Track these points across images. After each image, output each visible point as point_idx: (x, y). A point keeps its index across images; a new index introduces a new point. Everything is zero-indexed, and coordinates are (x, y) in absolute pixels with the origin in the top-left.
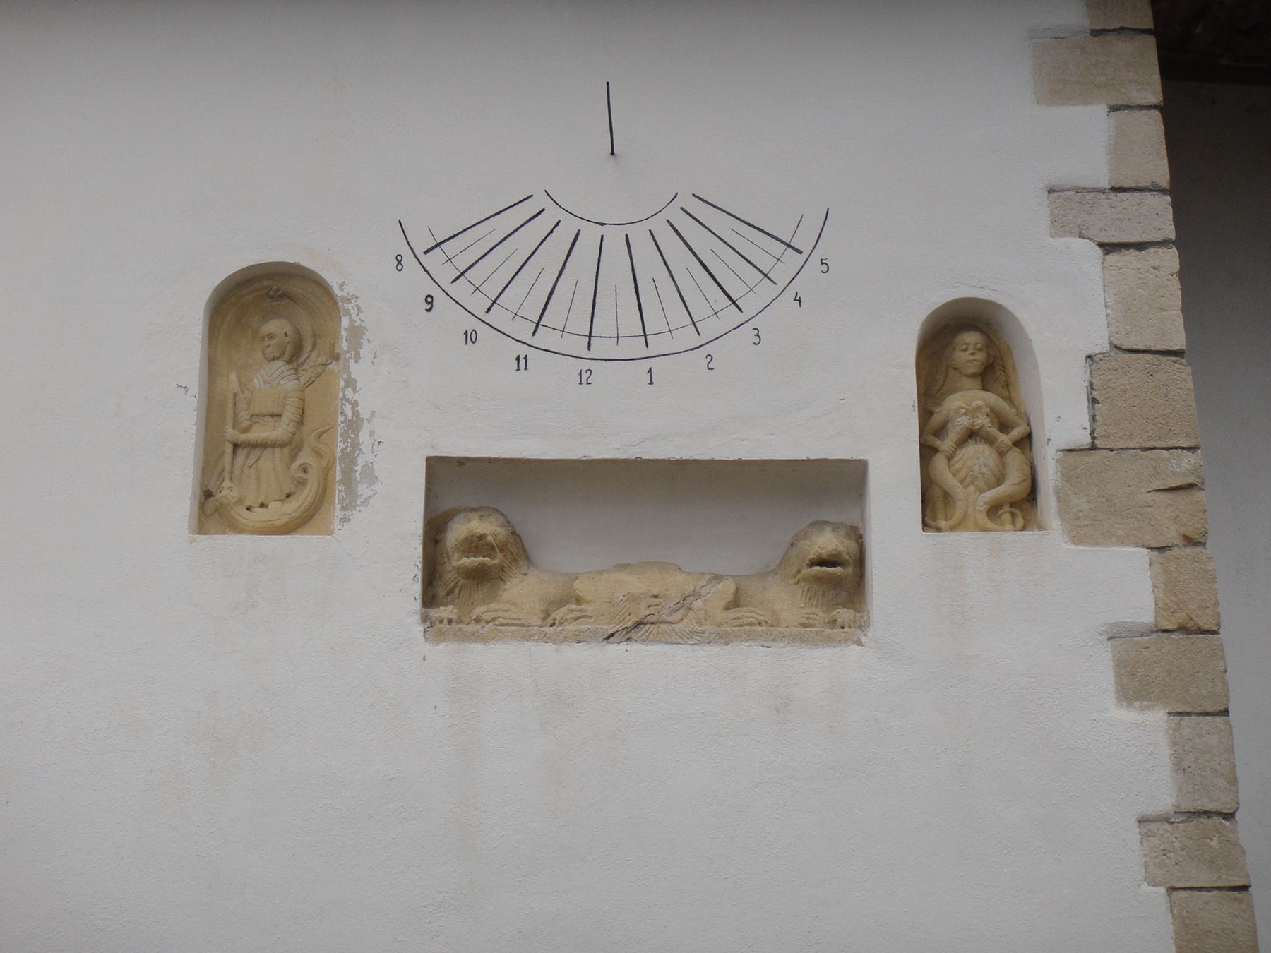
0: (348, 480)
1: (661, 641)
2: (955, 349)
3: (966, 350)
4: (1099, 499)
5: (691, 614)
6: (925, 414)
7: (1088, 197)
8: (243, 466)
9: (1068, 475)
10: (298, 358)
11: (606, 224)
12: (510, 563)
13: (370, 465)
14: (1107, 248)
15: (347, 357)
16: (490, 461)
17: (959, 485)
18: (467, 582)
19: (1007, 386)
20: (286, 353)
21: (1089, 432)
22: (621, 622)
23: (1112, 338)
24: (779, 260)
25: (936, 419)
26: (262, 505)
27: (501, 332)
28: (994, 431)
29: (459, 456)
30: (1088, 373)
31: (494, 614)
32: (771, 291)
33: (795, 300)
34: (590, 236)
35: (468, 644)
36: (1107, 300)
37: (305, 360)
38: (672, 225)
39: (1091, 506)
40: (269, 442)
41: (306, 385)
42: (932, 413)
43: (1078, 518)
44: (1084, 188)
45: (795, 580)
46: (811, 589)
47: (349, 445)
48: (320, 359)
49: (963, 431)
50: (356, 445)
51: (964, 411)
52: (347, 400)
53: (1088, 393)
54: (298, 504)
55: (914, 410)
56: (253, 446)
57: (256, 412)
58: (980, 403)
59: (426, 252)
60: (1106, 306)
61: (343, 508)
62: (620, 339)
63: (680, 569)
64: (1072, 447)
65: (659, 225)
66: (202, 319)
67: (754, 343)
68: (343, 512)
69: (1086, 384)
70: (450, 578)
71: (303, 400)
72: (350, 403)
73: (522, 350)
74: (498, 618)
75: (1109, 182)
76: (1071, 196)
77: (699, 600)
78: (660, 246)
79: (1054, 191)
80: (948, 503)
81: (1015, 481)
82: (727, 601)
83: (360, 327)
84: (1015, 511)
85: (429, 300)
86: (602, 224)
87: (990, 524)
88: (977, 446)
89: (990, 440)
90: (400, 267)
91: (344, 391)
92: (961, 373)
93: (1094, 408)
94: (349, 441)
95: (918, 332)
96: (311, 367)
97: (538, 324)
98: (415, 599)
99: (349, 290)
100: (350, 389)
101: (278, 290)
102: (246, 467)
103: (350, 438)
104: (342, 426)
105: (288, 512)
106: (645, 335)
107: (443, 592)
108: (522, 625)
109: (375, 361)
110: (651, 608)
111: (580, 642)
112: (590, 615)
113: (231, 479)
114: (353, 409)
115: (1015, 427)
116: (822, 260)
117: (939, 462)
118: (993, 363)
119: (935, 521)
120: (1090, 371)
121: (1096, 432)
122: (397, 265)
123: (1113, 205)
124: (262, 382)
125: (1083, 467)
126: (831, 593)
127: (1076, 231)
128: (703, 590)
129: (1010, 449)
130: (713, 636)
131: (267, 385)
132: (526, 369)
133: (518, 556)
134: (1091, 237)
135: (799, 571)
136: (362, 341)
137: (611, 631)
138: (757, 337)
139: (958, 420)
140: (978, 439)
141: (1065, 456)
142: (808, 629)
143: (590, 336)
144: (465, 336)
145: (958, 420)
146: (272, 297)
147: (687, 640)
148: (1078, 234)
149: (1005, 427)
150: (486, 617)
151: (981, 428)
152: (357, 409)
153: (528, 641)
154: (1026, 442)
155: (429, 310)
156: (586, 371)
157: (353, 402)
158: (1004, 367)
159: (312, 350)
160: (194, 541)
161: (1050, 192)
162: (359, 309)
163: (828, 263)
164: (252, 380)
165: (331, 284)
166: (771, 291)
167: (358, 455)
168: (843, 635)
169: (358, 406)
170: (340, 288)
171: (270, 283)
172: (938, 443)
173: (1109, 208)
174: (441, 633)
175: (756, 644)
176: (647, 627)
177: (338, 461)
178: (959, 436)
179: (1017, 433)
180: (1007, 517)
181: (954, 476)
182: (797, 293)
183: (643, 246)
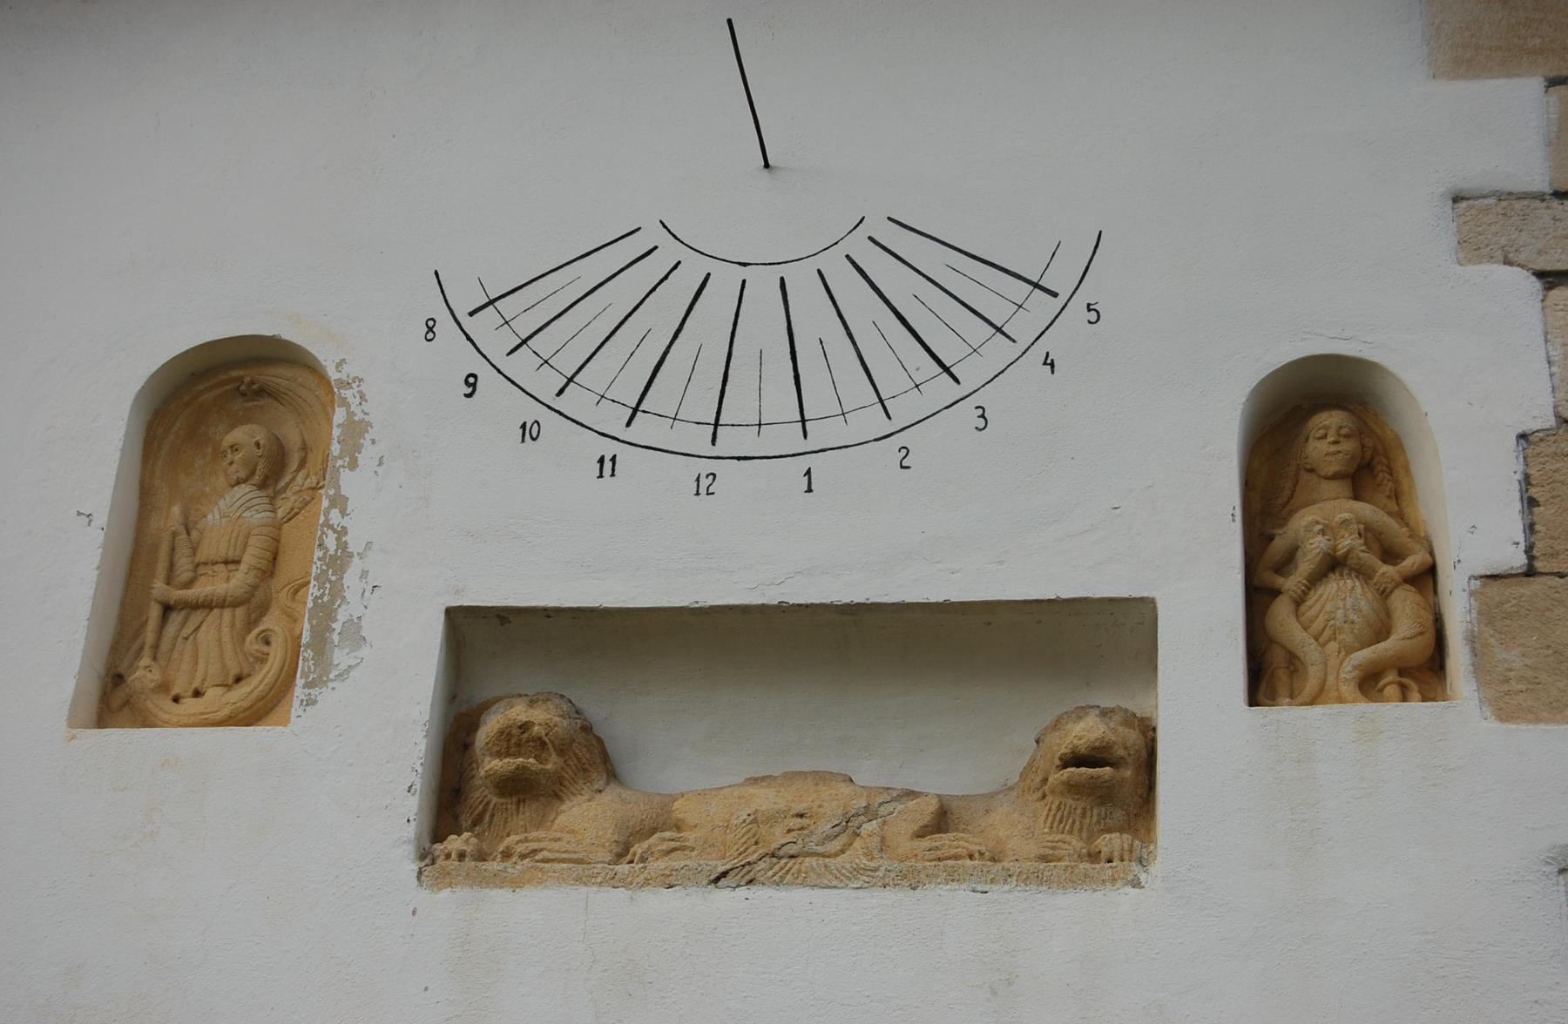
0: (321, 643)
1: (804, 884)
2: (1307, 440)
3: (1325, 437)
4: (1541, 651)
5: (857, 843)
7: (1517, 206)
8: (176, 638)
9: (1487, 614)
10: (277, 481)
11: (750, 264)
12: (576, 774)
13: (356, 621)
14: (1550, 279)
15: (338, 465)
16: (548, 613)
17: (1313, 641)
18: (502, 800)
19: (1397, 498)
20: (258, 472)
21: (1524, 548)
22: (740, 854)
23: (1560, 409)
24: (1020, 306)
25: (1280, 544)
26: (197, 694)
27: (577, 423)
28: (1371, 559)
29: (499, 605)
30: (1521, 460)
31: (534, 845)
32: (1007, 351)
33: (1045, 363)
34: (724, 284)
35: (487, 890)
36: (1551, 353)
37: (287, 485)
38: (853, 263)
39: (1528, 662)
40: (215, 598)
41: (285, 519)
42: (1271, 538)
43: (1507, 681)
44: (1510, 194)
45: (1039, 794)
46: (1063, 807)
47: (327, 592)
48: (309, 480)
49: (1318, 558)
50: (337, 592)
51: (1320, 527)
52: (331, 527)
53: (1521, 490)
54: (248, 689)
55: (1234, 520)
56: (194, 606)
57: (202, 560)
58: (1346, 515)
59: (471, 314)
60: (1549, 362)
61: (308, 685)
62: (762, 427)
63: (851, 781)
64: (1496, 572)
65: (826, 262)
66: (126, 420)
67: (977, 428)
68: (307, 691)
69: (1519, 476)
70: (478, 798)
71: (277, 541)
72: (335, 531)
73: (608, 448)
74: (542, 850)
75: (1550, 184)
76: (1490, 205)
77: (874, 822)
79: (1463, 199)
80: (1296, 671)
81: (1407, 634)
82: (921, 824)
83: (362, 421)
84: (1404, 680)
85: (471, 382)
86: (745, 265)
89: (1364, 573)
90: (430, 336)
91: (327, 513)
93: (1531, 513)
94: (328, 585)
95: (1241, 407)
96: (295, 493)
97: (635, 410)
98: (408, 821)
99: (349, 370)
100: (337, 510)
101: (252, 383)
102: (179, 639)
103: (330, 582)
104: (319, 563)
105: (232, 701)
107: (466, 821)
108: (579, 862)
109: (380, 470)
110: (793, 833)
111: (671, 887)
112: (693, 846)
113: (155, 658)
114: (338, 539)
115: (1409, 555)
116: (1089, 305)
117: (1281, 611)
118: (1371, 460)
120: (1525, 458)
121: (1536, 549)
122: (427, 333)
123: (1557, 218)
124: (217, 516)
125: (1514, 602)
126: (1096, 811)
127: (1499, 255)
128: (882, 808)
129: (1397, 586)
130: (892, 875)
131: (224, 520)
132: (613, 475)
133: (590, 764)
134: (1523, 263)
135: (1045, 780)
136: (362, 441)
137: (721, 869)
138: (982, 419)
139: (1311, 542)
140: (1346, 572)
141: (1484, 586)
142: (1052, 864)
144: (521, 430)
146: (244, 395)
147: (847, 882)
148: (1502, 258)
149: (1390, 555)
150: (521, 848)
151: (1348, 552)
152: (344, 539)
153: (585, 884)
154: (1426, 578)
155: (469, 396)
156: (707, 476)
157: (339, 529)
159: (298, 470)
160: (73, 737)
161: (1457, 199)
162: (362, 397)
163: (1098, 309)
164: (205, 516)
165: (324, 363)
166: (1007, 351)
167: (339, 606)
168: (1110, 872)
169: (346, 533)
170: (337, 367)
171: (241, 373)
172: (1280, 581)
173: (1552, 222)
174: (445, 873)
175: (964, 886)
176: (783, 862)
177: (307, 615)
178: (1312, 566)
179: (1412, 562)
180: (1392, 690)
181: (1306, 629)
182: (1048, 353)
183: (808, 297)
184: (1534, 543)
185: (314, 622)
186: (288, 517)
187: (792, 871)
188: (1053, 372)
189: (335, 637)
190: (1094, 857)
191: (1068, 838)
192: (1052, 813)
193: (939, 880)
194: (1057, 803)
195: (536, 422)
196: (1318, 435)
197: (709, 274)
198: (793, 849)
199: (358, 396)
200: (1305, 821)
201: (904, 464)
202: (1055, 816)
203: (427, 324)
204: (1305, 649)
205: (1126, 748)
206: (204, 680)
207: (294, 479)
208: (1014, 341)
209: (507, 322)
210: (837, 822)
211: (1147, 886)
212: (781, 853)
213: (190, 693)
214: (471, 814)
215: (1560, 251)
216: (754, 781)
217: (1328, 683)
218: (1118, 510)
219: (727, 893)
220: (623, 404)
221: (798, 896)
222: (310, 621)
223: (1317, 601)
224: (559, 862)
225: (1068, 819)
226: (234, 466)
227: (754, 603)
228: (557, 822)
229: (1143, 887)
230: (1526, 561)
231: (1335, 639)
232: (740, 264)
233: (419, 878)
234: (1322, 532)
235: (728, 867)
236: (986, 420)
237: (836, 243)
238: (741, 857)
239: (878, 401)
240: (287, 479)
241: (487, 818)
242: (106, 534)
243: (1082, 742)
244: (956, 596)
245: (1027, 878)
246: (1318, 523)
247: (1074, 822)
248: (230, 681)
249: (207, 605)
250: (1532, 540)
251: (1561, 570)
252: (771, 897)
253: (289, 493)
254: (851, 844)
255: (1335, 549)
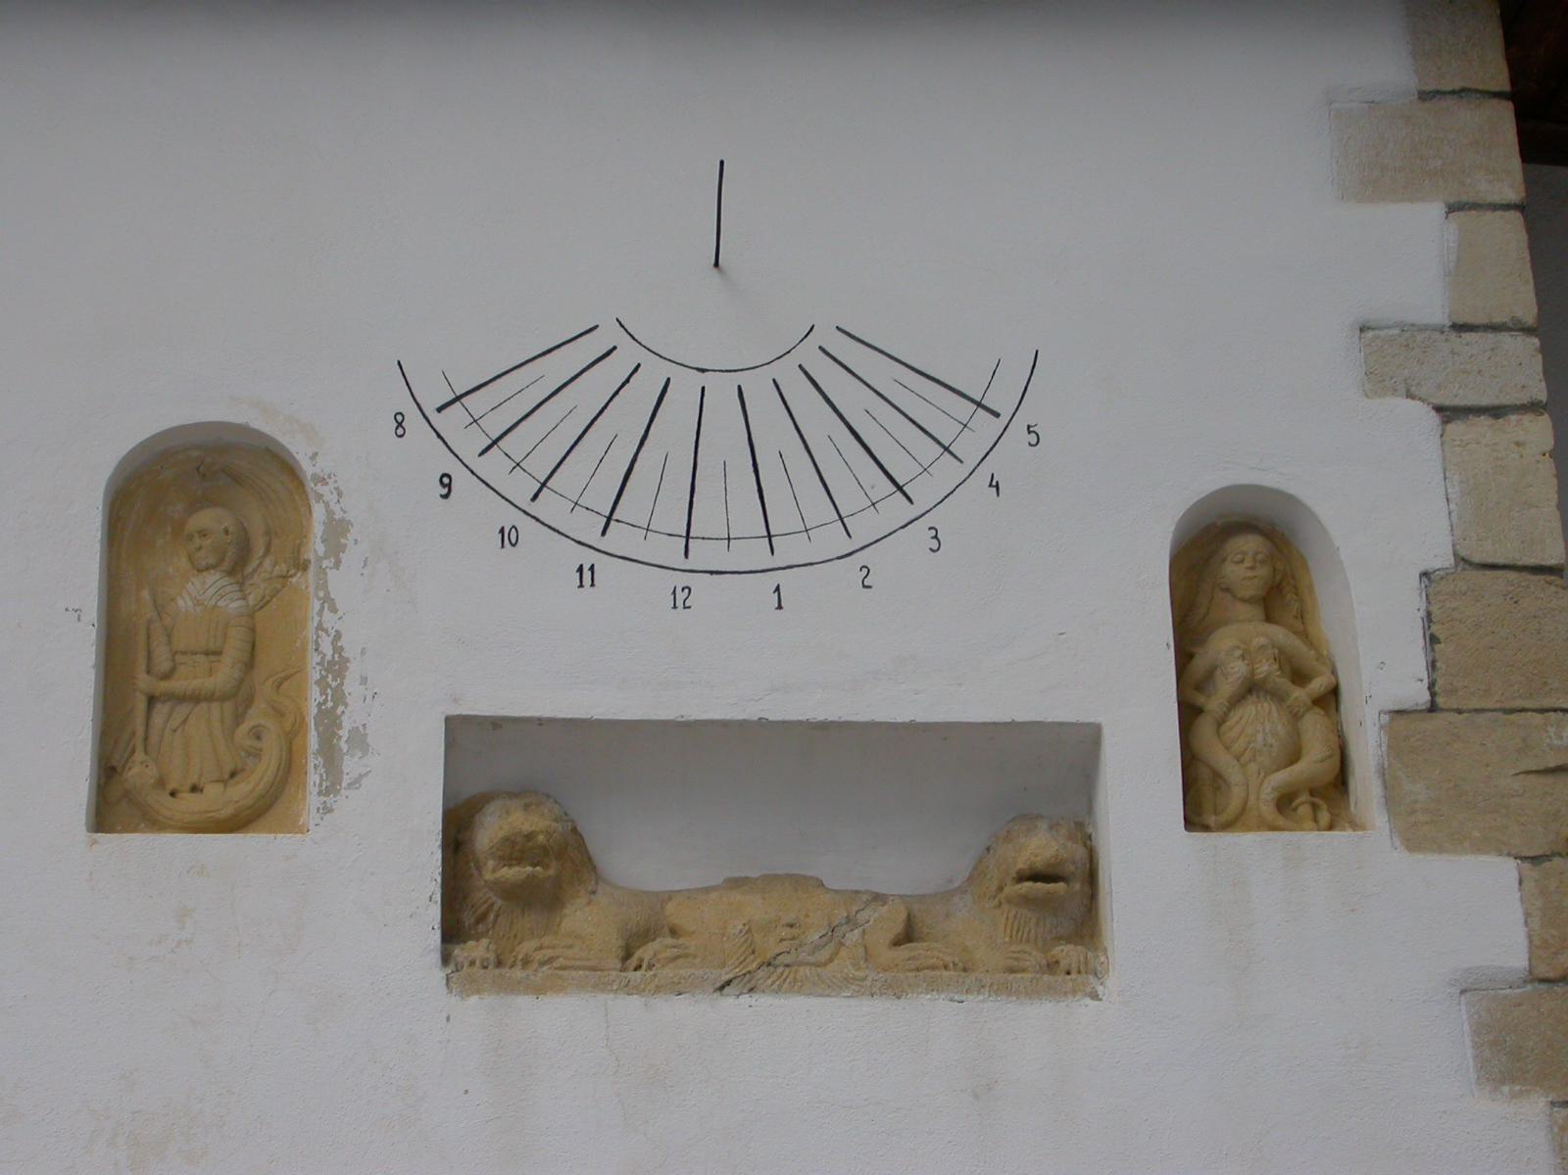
2: (1224, 560)
3: (1242, 561)
5: (843, 953)
6: (1184, 658)
11: (707, 370)
17: (1235, 762)
20: (227, 559)
21: (1427, 685)
22: (741, 963)
25: (1199, 664)
26: (195, 789)
28: (1284, 683)
31: (549, 953)
36: (1449, 491)
37: (255, 570)
38: (806, 373)
42: (1191, 656)
44: (1413, 325)
45: (996, 901)
47: (329, 698)
48: (277, 567)
49: (1240, 682)
50: (339, 697)
59: (439, 410)
60: (1448, 500)
62: (732, 541)
65: (750, 383)
69: (1422, 613)
71: (253, 630)
73: (588, 557)
77: (856, 931)
78: (788, 403)
83: (342, 520)
84: (1316, 800)
85: (446, 482)
86: (703, 371)
87: (1281, 821)
88: (1259, 706)
89: (1278, 697)
90: (400, 431)
92: (1234, 596)
93: (1433, 650)
94: (329, 691)
98: (433, 929)
104: (318, 668)
106: (770, 536)
108: (593, 969)
109: (365, 571)
110: (784, 943)
113: (146, 751)
115: (1316, 677)
116: (1029, 427)
117: (1205, 728)
118: (1280, 583)
119: (1200, 815)
122: (397, 429)
123: (1456, 350)
129: (1308, 710)
132: (592, 585)
136: (343, 541)
137: (726, 978)
138: (935, 541)
140: (1262, 694)
141: (1392, 720)
143: (688, 537)
145: (1232, 665)
148: (1404, 391)
149: (1300, 677)
150: (539, 956)
151: (1265, 678)
158: (1295, 587)
160: (95, 842)
164: (172, 600)
169: (340, 637)
176: (780, 970)
179: (1318, 685)
180: (1305, 810)
181: (1227, 748)
182: (993, 475)
183: (680, 402)
184: (1436, 680)
185: (321, 729)
186: (261, 604)
187: (788, 980)
188: (998, 494)
189: (345, 747)
190: (1052, 966)
191: (1028, 948)
192: (1010, 922)
193: (920, 990)
194: (1014, 912)
195: (514, 527)
196: (1236, 559)
197: (597, 327)
198: (787, 959)
199: (335, 493)
200: (1241, 942)
201: (865, 583)
202: (1012, 924)
203: (395, 418)
204: (1230, 770)
205: (1074, 863)
206: (201, 776)
207: (260, 564)
208: (961, 462)
209: (475, 421)
210: (824, 932)
211: (1104, 998)
212: (777, 962)
213: (188, 787)
214: (474, 913)
215: (1457, 386)
216: (736, 883)
217: (1249, 803)
218: (1065, 636)
219: (731, 1000)
220: (597, 513)
221: (798, 1003)
222: (317, 729)
223: (1238, 722)
224: (575, 969)
225: (1024, 928)
226: (203, 551)
227: (736, 718)
228: (563, 925)
229: (1101, 1000)
230: (1430, 698)
231: (1255, 760)
232: (698, 369)
233: (447, 984)
234: (1243, 657)
235: (731, 976)
236: (938, 540)
237: (789, 352)
238: (741, 966)
239: (845, 520)
240: (254, 563)
241: (492, 916)
242: (97, 630)
243: (1039, 858)
244: (922, 717)
245: (998, 989)
246: (1238, 648)
247: (1030, 931)
248: (226, 777)
249: (195, 698)
250: (1434, 676)
251: (1460, 707)
252: (771, 1005)
253: (256, 578)
254: (837, 954)
255: (1253, 674)
